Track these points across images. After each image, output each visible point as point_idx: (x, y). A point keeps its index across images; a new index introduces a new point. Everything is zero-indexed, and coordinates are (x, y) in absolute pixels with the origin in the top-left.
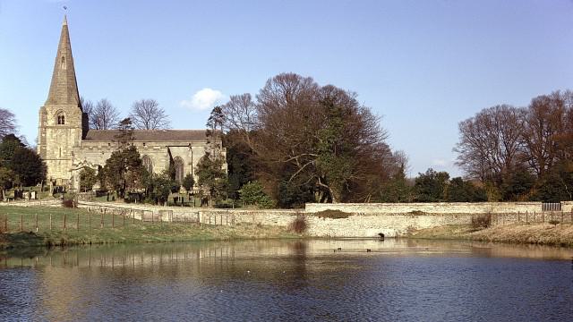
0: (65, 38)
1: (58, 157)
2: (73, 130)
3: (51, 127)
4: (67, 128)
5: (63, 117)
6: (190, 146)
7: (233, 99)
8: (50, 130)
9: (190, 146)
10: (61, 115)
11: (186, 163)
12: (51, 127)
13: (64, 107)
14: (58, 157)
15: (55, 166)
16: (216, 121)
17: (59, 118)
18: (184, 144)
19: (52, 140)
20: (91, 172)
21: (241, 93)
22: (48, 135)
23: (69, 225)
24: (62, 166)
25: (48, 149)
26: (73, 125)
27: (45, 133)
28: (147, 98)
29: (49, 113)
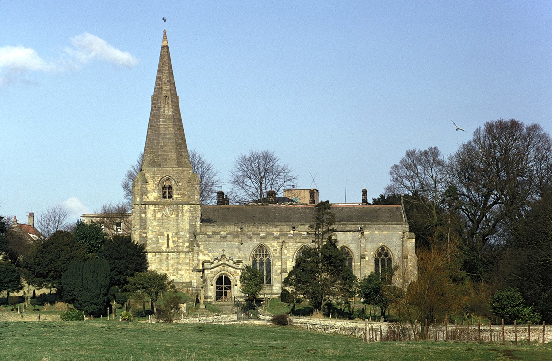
0: (165, 75)
1: (164, 248)
2: (186, 208)
3: (154, 204)
4: (177, 204)
5: (170, 187)
6: (361, 231)
7: (410, 154)
8: (152, 208)
9: (361, 231)
10: (167, 184)
11: (356, 256)
12: (154, 204)
13: (172, 172)
14: (164, 248)
15: (161, 261)
16: (521, 206)
17: (164, 187)
18: (352, 227)
19: (155, 223)
20: (396, 166)
21: (424, 147)
22: (149, 215)
23: (323, 229)
24: (171, 262)
25: (150, 235)
26: (186, 199)
27: (145, 213)
28: (260, 149)
29: (150, 181)
